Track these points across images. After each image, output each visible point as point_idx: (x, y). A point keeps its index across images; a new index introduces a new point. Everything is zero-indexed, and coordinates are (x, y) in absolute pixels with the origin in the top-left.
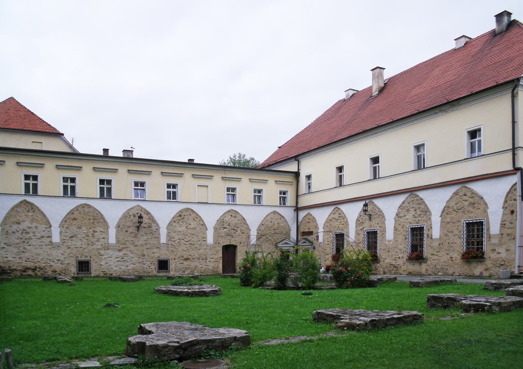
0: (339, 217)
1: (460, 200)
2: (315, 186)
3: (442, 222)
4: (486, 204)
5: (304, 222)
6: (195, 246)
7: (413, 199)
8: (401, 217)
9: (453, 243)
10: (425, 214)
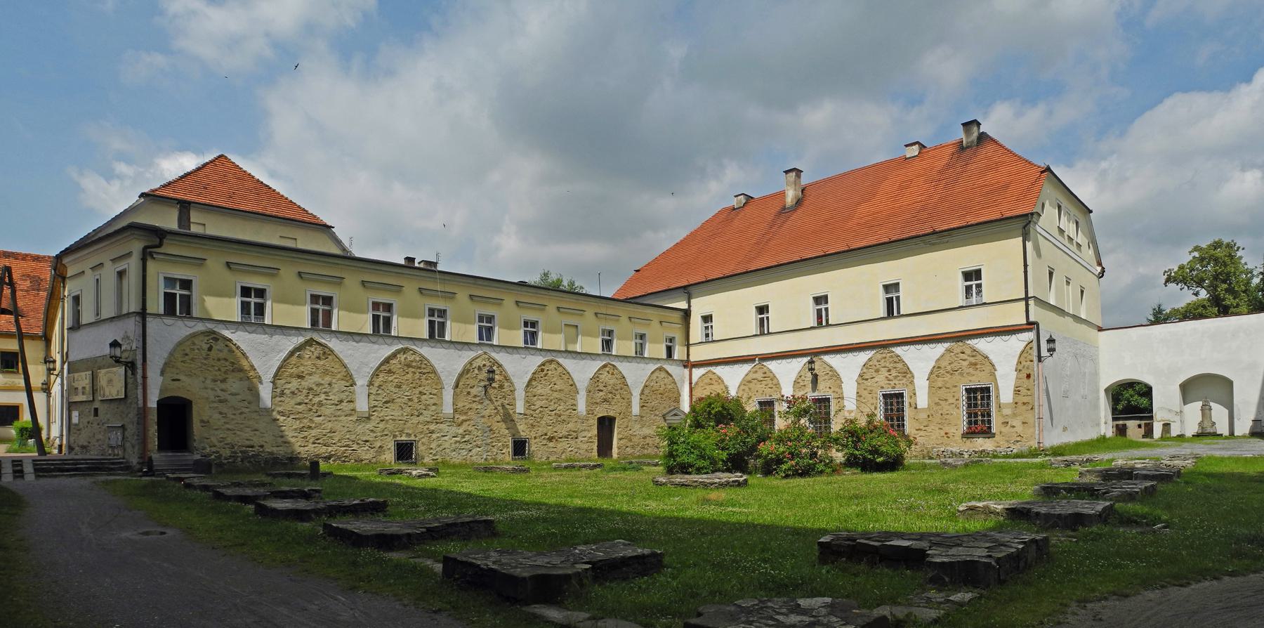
0: (765, 377)
1: (956, 359)
2: (718, 332)
3: (930, 387)
4: (993, 366)
5: (701, 384)
6: (562, 417)
7: (884, 355)
8: (867, 380)
9: (948, 414)
10: (905, 377)
